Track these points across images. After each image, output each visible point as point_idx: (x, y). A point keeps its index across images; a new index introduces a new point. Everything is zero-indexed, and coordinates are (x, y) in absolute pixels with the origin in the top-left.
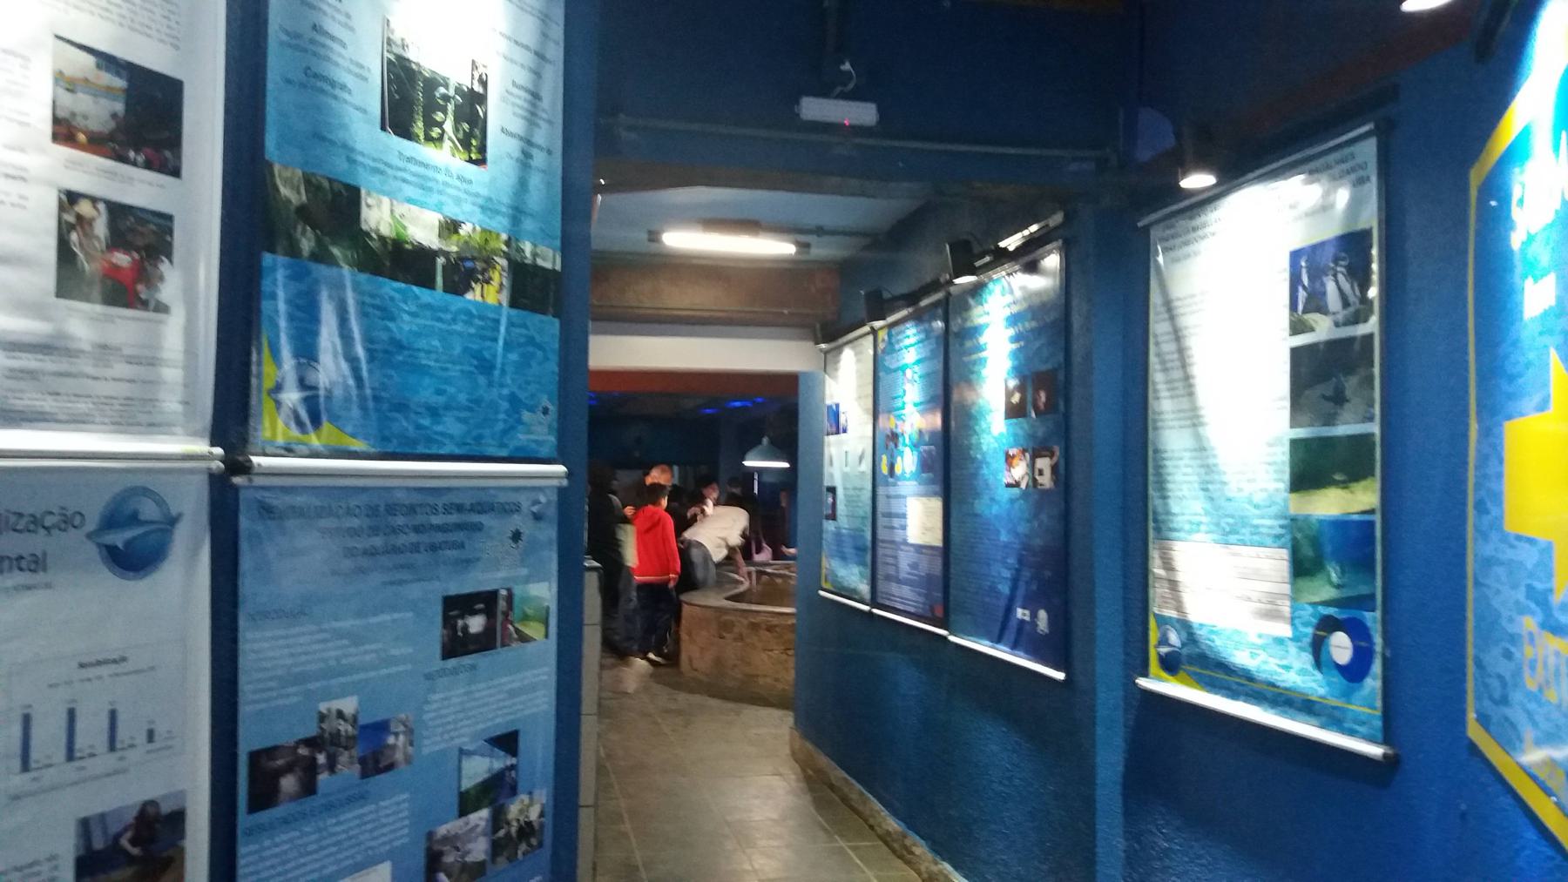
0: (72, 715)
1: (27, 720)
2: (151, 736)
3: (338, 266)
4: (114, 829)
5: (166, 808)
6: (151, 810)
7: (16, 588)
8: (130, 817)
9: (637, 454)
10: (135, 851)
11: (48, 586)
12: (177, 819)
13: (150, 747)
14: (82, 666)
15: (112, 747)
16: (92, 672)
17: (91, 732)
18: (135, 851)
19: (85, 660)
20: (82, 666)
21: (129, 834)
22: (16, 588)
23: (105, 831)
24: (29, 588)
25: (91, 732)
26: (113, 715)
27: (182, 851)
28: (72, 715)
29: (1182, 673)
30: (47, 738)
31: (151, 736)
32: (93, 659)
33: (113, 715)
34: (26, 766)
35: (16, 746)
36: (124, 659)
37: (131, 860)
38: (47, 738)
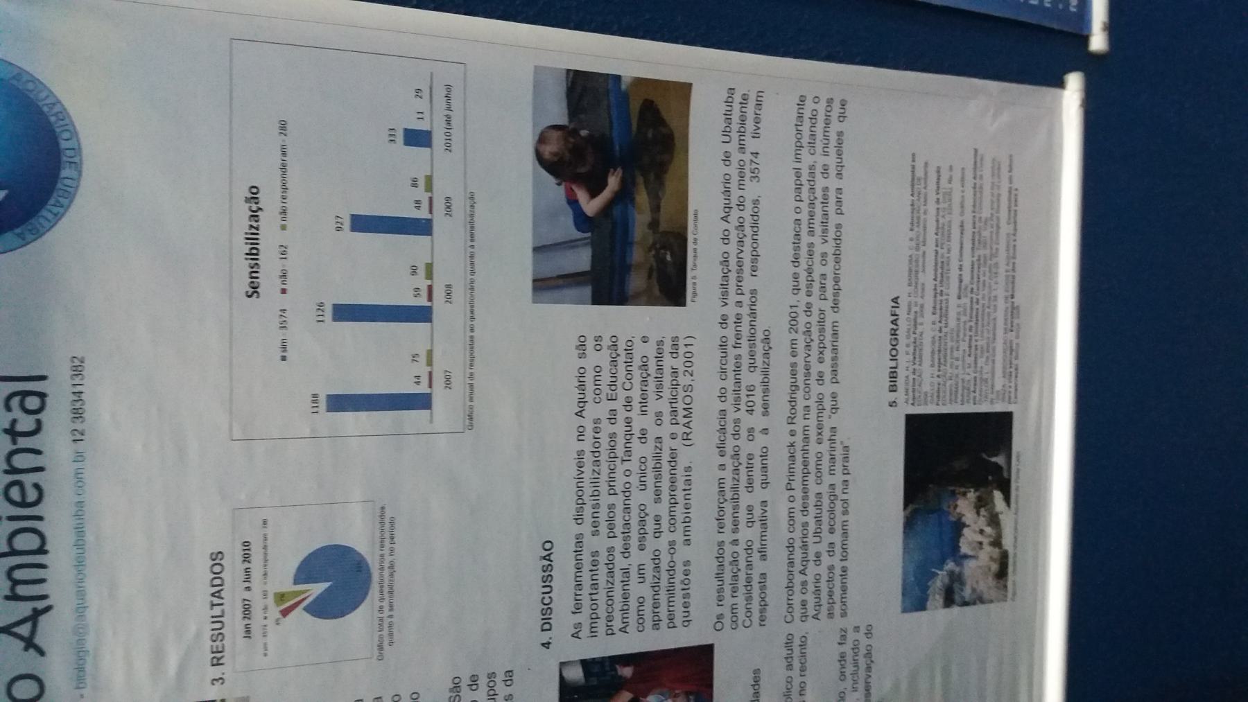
0: (345, 313)
1: (339, 403)
2: (417, 138)
3: (296, 582)
4: (566, 228)
5: (558, 113)
6: (549, 150)
7: (78, 436)
8: (555, 191)
9: (584, 133)
10: (613, 182)
11: (77, 370)
12: (583, 88)
13: (438, 139)
14: (254, 291)
15: (422, 227)
16: (269, 280)
17: (384, 270)
18: (613, 182)
19: (243, 284)
20: (254, 291)
21: (582, 196)
22: (78, 436)
23: (570, 244)
24: (78, 414)
25: (384, 270)
26: (362, 224)
27: (639, 82)
28: (345, 313)
29: (1085, 33)
30: (380, 358)
31: (417, 138)
32: (243, 266)
33: (362, 224)
34: (421, 402)
35: (385, 419)
36: (254, 196)
37: (624, 195)
38: (380, 358)
